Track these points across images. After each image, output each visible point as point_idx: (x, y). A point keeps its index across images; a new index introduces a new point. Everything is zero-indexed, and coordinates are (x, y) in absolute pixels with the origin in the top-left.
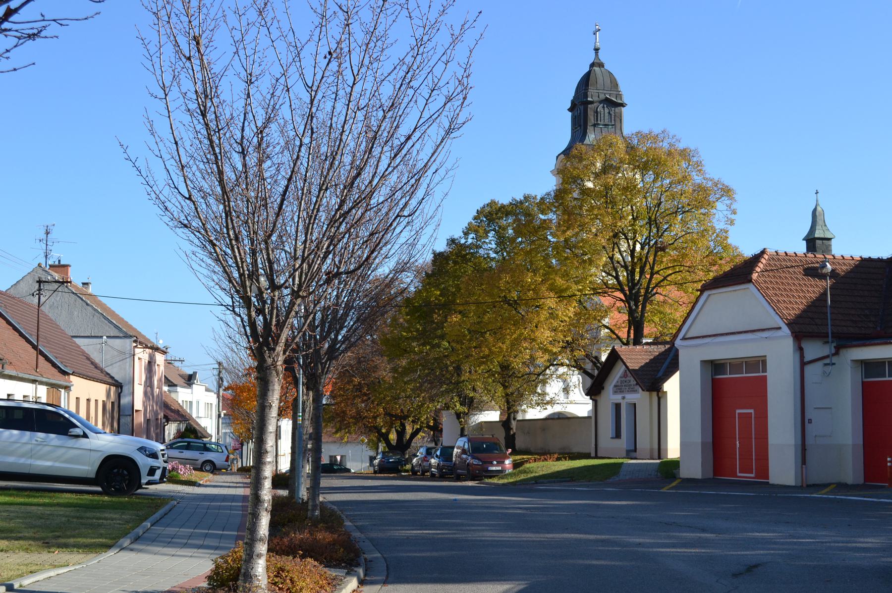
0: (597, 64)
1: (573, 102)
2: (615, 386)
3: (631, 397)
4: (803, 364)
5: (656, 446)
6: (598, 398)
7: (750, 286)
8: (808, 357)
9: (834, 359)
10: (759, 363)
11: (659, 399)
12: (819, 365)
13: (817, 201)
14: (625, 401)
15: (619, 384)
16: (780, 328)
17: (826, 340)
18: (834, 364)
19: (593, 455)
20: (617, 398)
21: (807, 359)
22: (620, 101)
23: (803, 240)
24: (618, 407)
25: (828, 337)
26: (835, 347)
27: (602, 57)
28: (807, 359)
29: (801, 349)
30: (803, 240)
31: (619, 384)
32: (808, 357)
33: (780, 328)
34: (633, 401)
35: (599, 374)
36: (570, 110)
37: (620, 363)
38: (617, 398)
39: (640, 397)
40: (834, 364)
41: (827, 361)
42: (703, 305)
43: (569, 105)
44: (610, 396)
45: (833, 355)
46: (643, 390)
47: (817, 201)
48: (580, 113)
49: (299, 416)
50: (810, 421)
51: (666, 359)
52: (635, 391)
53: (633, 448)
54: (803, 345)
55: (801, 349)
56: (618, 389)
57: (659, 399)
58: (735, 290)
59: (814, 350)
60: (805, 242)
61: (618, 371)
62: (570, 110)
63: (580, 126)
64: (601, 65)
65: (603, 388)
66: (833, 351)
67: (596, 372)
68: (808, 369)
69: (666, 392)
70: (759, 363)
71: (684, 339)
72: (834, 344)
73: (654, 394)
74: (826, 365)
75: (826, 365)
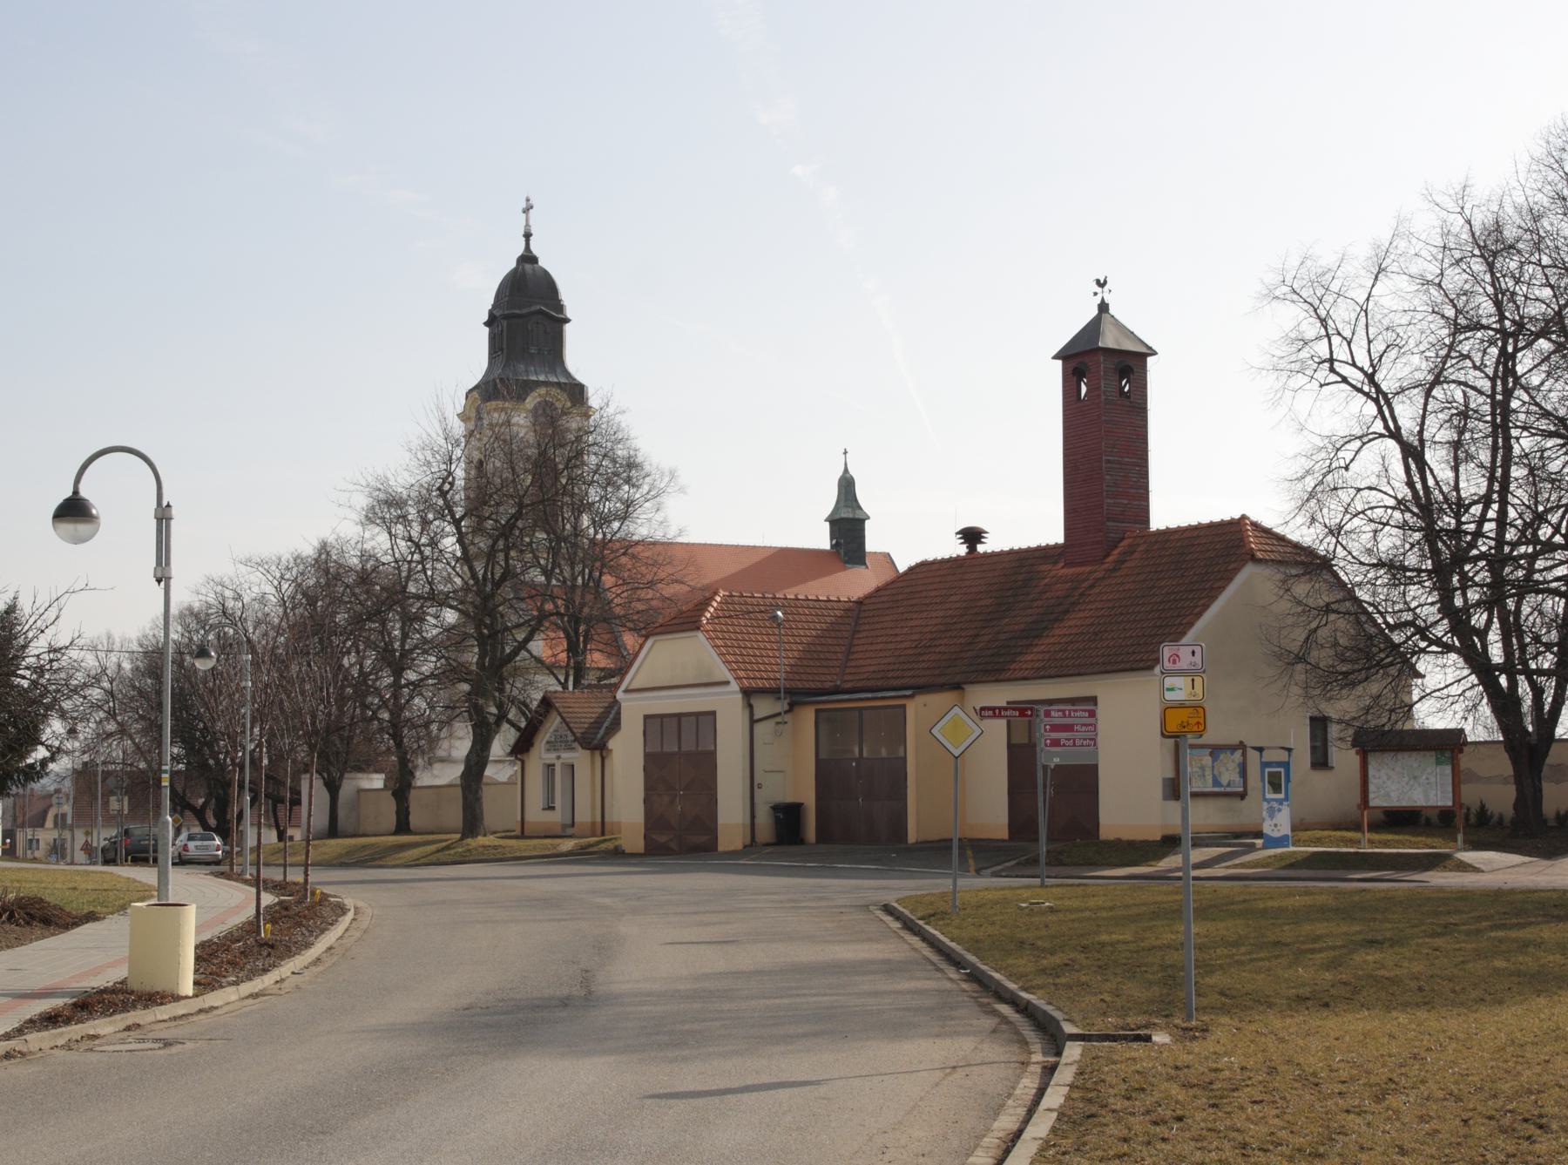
0: (528, 258)
1: (491, 313)
2: (548, 742)
3: (567, 756)
4: (753, 722)
5: (599, 819)
6: (524, 757)
7: (700, 635)
8: (758, 714)
9: (787, 717)
10: (707, 719)
11: (603, 759)
12: (770, 724)
13: (846, 464)
14: (561, 761)
15: (553, 739)
16: (727, 683)
17: (777, 695)
18: (786, 723)
19: (518, 832)
20: (550, 757)
21: (756, 717)
22: (560, 316)
23: (826, 520)
24: (550, 768)
25: (780, 692)
26: (789, 704)
27: (536, 249)
28: (756, 717)
29: (751, 707)
30: (826, 520)
31: (553, 739)
32: (758, 714)
33: (727, 683)
34: (570, 761)
35: (526, 727)
36: (487, 324)
37: (554, 714)
38: (550, 757)
39: (580, 758)
40: (786, 723)
41: (779, 719)
42: (648, 653)
43: (486, 318)
44: (540, 755)
45: (786, 712)
46: (583, 748)
47: (846, 464)
48: (502, 331)
49: (166, 772)
50: (760, 786)
51: (610, 712)
52: (572, 749)
53: (570, 822)
54: (752, 702)
55: (751, 707)
56: (552, 746)
57: (603, 759)
58: (508, 831)
59: (763, 707)
60: (828, 523)
61: (553, 724)
62: (487, 324)
63: (502, 350)
64: (534, 260)
65: (532, 745)
66: (786, 707)
67: (523, 724)
68: (758, 728)
69: (611, 750)
70: (707, 719)
71: (627, 691)
72: (788, 701)
73: (597, 753)
74: (778, 723)
75: (778, 723)
